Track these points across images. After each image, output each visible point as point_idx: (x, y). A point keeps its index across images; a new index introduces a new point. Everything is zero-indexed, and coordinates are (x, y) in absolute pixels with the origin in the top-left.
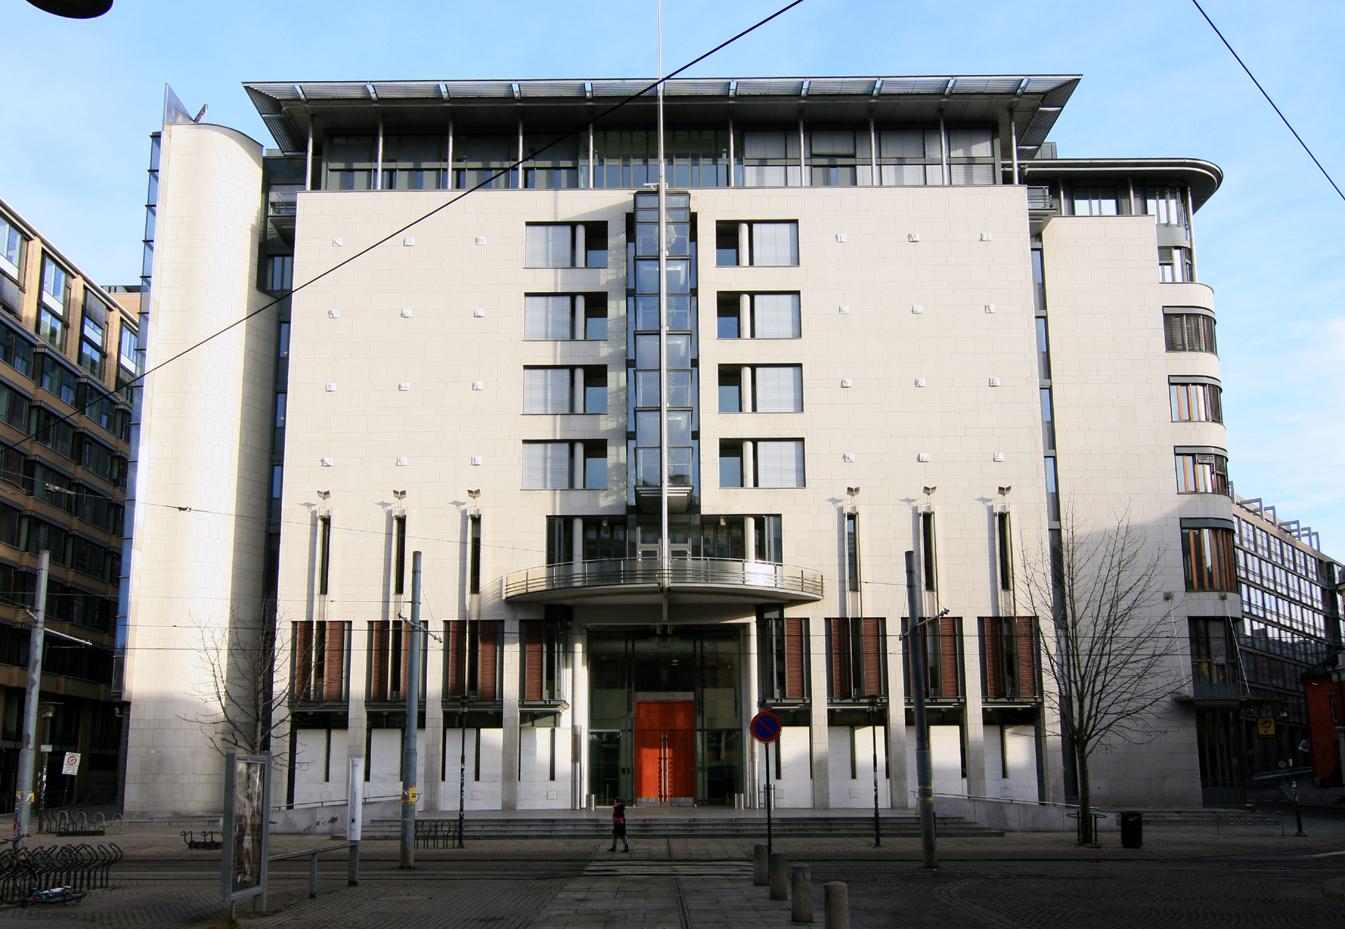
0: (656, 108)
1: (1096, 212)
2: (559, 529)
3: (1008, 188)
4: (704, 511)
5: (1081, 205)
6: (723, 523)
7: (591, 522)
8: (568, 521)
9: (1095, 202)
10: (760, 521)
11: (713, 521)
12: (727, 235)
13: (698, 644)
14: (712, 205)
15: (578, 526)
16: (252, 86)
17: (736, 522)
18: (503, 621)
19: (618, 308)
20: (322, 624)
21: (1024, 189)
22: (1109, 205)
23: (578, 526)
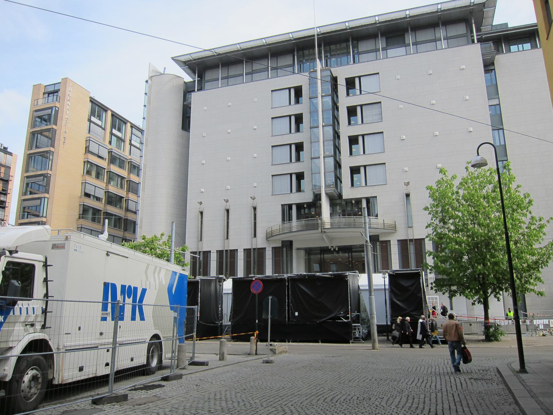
0: (314, 39)
1: (521, 49)
2: (287, 209)
3: (473, 45)
4: (344, 198)
5: (513, 48)
6: (353, 202)
7: (300, 206)
8: (290, 206)
9: (520, 46)
10: (368, 200)
11: (349, 202)
12: (350, 83)
13: (350, 254)
14: (343, 72)
15: (294, 208)
16: (177, 58)
17: (358, 201)
18: (265, 248)
19: (496, 110)
20: (226, 251)
21: (479, 44)
22: (527, 46)
23: (294, 208)
